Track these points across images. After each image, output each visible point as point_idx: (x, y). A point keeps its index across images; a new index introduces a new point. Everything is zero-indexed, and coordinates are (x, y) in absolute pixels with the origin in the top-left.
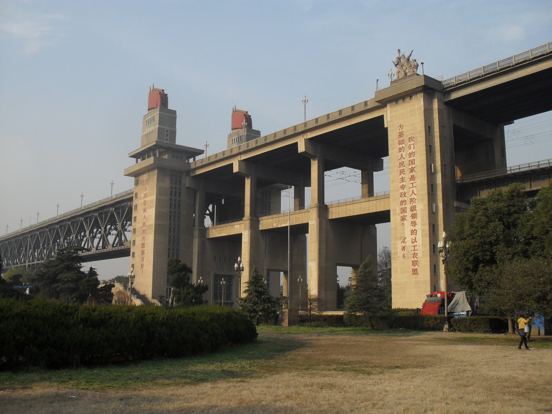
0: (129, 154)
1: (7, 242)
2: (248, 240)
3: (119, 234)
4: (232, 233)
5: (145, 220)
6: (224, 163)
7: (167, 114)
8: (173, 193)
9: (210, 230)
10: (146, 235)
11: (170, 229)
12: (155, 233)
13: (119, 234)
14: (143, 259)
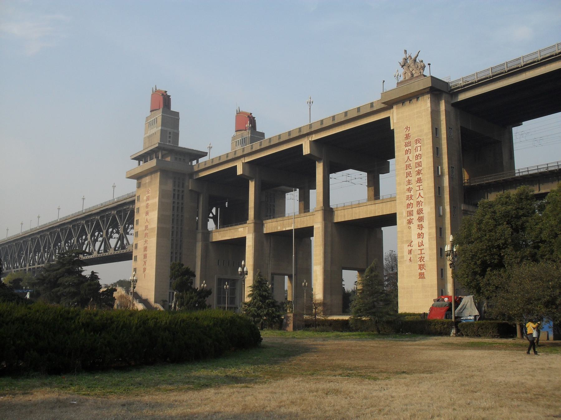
0: (131, 156)
1: (7, 246)
2: (252, 243)
3: (121, 237)
4: (236, 236)
5: (147, 224)
6: (228, 166)
7: (170, 116)
8: (176, 196)
9: (213, 233)
10: (148, 239)
11: (173, 232)
12: (157, 237)
13: (121, 237)
14: (145, 262)
